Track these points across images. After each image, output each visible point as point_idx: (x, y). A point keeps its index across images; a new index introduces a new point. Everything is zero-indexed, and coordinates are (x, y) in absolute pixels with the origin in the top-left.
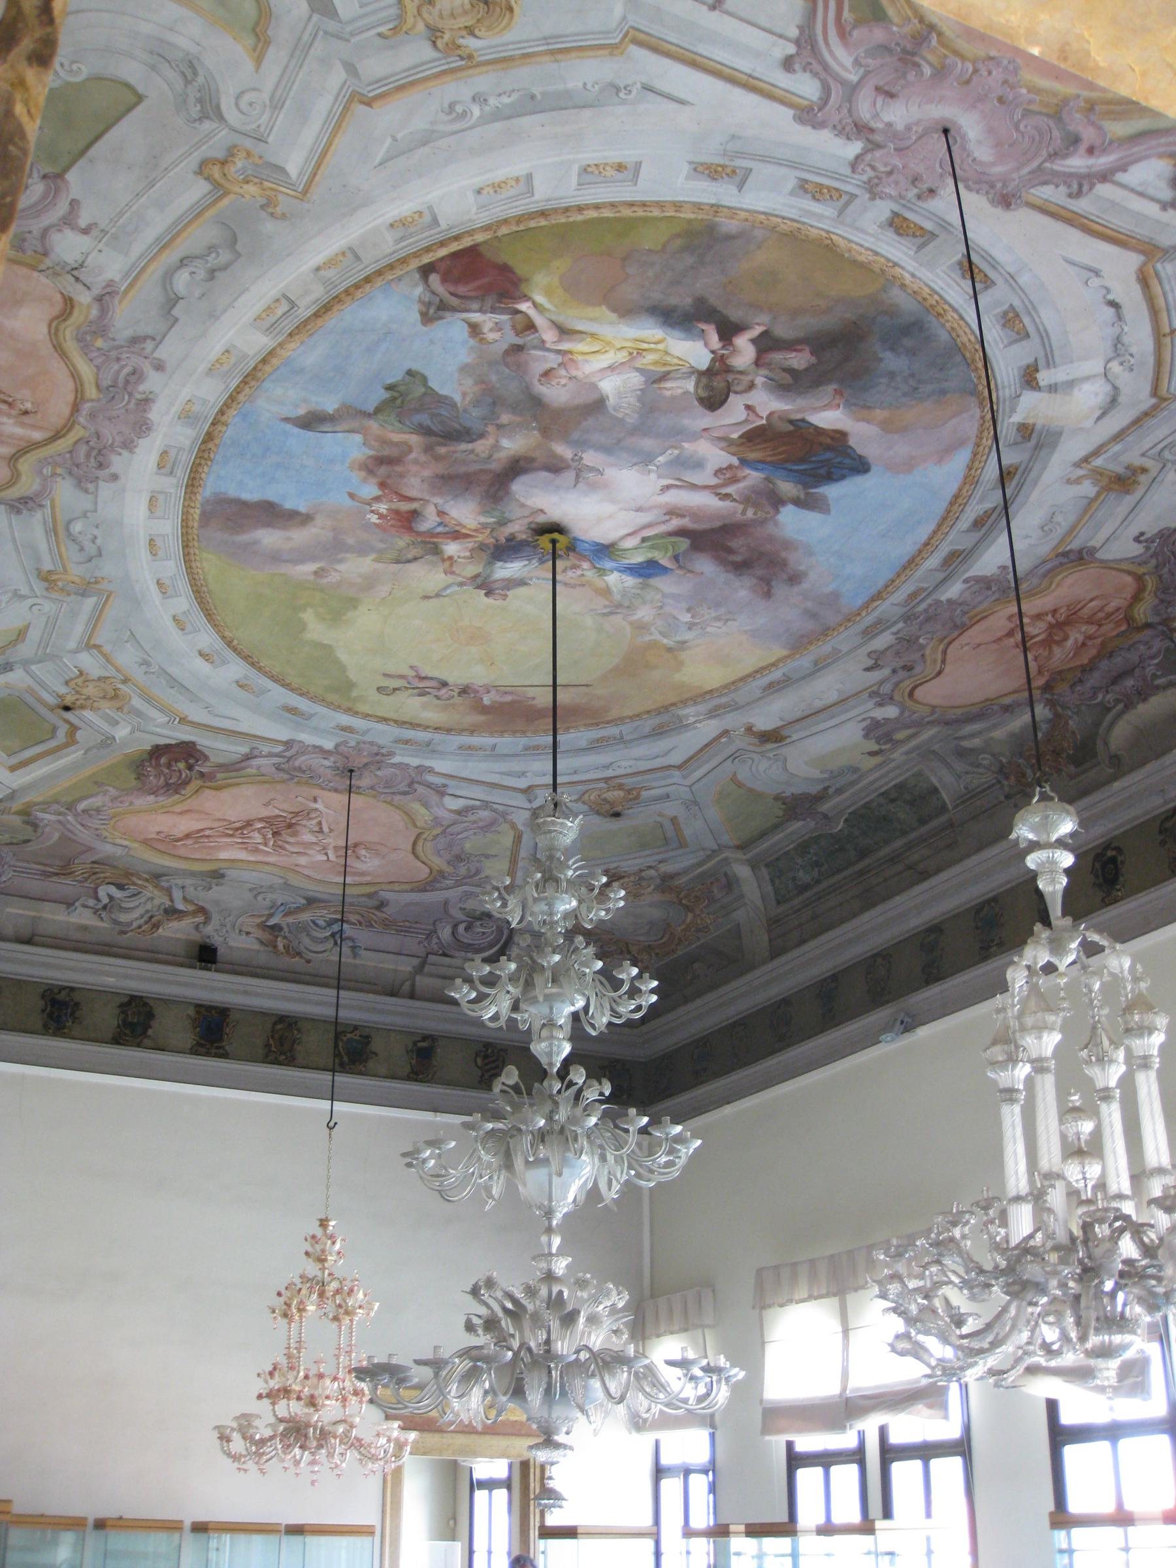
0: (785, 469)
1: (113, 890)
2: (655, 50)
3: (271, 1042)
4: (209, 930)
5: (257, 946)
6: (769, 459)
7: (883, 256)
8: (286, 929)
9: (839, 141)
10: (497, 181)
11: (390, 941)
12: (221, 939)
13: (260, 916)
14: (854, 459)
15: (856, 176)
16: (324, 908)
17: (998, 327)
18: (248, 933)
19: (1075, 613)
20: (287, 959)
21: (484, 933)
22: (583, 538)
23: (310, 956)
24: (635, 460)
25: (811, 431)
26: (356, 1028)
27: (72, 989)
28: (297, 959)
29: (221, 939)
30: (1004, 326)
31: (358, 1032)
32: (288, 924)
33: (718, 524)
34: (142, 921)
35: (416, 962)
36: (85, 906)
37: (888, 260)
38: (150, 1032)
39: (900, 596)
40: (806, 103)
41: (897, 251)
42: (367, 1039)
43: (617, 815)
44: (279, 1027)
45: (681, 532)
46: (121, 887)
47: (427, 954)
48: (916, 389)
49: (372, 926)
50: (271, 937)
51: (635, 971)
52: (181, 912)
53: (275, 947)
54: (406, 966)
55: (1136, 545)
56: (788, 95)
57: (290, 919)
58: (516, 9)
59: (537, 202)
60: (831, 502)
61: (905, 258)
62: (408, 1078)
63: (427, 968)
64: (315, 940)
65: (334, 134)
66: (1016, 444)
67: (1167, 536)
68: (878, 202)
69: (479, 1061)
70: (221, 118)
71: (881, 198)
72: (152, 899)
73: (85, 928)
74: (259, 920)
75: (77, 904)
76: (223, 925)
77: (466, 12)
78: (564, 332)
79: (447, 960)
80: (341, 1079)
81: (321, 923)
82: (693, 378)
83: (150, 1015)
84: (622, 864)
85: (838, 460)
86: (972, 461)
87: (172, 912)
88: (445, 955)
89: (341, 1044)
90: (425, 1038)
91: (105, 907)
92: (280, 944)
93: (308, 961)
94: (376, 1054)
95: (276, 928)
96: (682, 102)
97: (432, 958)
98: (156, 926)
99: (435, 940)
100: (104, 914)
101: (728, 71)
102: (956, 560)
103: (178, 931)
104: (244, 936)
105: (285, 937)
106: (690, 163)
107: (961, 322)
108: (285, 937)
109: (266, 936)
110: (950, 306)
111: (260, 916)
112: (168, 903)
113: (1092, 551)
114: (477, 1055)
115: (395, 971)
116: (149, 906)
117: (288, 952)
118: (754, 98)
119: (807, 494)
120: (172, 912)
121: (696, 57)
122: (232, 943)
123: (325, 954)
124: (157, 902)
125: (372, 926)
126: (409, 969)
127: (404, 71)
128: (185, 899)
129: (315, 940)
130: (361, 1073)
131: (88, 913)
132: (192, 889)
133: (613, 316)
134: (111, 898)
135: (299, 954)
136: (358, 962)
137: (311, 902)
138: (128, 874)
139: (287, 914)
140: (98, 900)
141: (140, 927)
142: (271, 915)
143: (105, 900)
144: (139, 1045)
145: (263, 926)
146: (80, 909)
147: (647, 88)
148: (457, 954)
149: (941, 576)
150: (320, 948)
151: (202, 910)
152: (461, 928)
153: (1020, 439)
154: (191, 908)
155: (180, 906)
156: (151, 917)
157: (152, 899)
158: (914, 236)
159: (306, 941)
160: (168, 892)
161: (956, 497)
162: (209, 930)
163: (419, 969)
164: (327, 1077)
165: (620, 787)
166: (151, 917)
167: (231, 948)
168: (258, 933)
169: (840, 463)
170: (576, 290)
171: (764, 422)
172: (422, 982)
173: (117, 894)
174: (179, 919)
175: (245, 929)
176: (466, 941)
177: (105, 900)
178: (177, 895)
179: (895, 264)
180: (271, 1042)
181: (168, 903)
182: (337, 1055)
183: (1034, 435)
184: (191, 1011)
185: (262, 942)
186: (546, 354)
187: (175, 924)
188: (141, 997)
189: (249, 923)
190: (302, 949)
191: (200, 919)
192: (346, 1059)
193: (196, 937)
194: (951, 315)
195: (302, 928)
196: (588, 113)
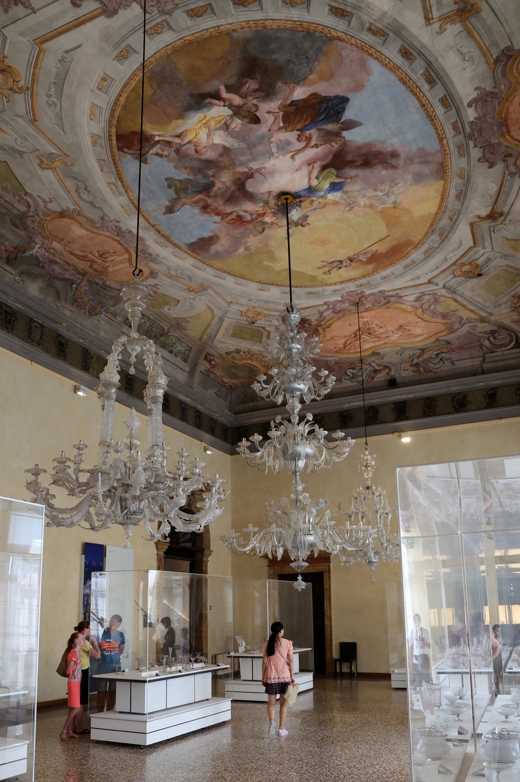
0: (318, 122)
1: (351, 371)
2: (48, 40)
3: (425, 409)
4: (392, 373)
5: (413, 374)
6: (307, 123)
7: (211, 28)
8: (421, 363)
9: (129, 10)
10: (89, 112)
11: (465, 354)
12: (398, 375)
13: (409, 362)
14: (336, 99)
16: (430, 351)
18: (407, 370)
20: (426, 374)
21: (504, 338)
22: (299, 190)
24: (267, 156)
25: (302, 102)
26: (460, 393)
27: (348, 410)
28: (430, 373)
29: (398, 375)
30: (293, 6)
31: (461, 395)
32: (421, 361)
34: (367, 378)
35: (480, 359)
36: (345, 379)
37: (214, 28)
38: (378, 418)
39: (449, 132)
41: (207, 23)
42: (465, 397)
43: (480, 275)
44: (427, 402)
45: (324, 168)
46: (353, 369)
47: (484, 354)
48: (308, 58)
49: (454, 351)
50: (417, 368)
52: (379, 370)
53: (420, 371)
54: (477, 362)
56: (93, 13)
57: (421, 359)
58: (11, 65)
59: (107, 108)
60: (356, 120)
61: (214, 22)
62: (486, 408)
63: (487, 360)
64: (435, 364)
65: (45, 135)
71: (173, 12)
72: (366, 369)
73: (347, 387)
74: (409, 364)
75: (342, 379)
76: (397, 370)
77: (6, 78)
78: (179, 136)
79: (494, 354)
83: (377, 412)
85: (330, 104)
88: (492, 352)
89: (454, 402)
90: (491, 389)
91: (352, 377)
92: (422, 369)
93: (435, 373)
94: (470, 402)
95: (417, 364)
96: (79, 46)
97: (487, 355)
98: (373, 378)
99: (484, 348)
100: (353, 380)
103: (381, 377)
104: (406, 371)
105: (422, 367)
107: (276, 21)
108: (422, 367)
109: (414, 368)
110: (262, 20)
111: (409, 362)
112: (373, 369)
115: (473, 365)
116: (367, 372)
117: (426, 372)
118: (89, 25)
119: (342, 123)
120: (376, 371)
121: (59, 30)
122: (403, 376)
123: (441, 368)
124: (369, 369)
125: (454, 351)
126: (479, 363)
127: (26, 105)
128: (377, 365)
129: (435, 364)
130: (465, 411)
132: (377, 361)
134: (353, 373)
135: (430, 371)
136: (456, 367)
137: (423, 350)
139: (418, 358)
140: (349, 376)
141: (367, 380)
142: (413, 360)
143: (351, 375)
144: (375, 424)
145: (412, 365)
146: (344, 381)
148: (497, 350)
149: (453, 112)
150: (438, 366)
151: (386, 367)
154: (382, 368)
155: (378, 368)
156: (370, 376)
157: (366, 369)
158: (205, 11)
159: (431, 365)
160: (370, 364)
162: (392, 373)
163: (483, 361)
166: (370, 376)
167: (403, 377)
168: (411, 369)
169: (332, 104)
170: (166, 119)
171: (282, 113)
173: (354, 371)
174: (380, 373)
175: (406, 368)
176: (498, 343)
177: (351, 375)
178: (374, 365)
179: (218, 27)
180: (425, 409)
181: (373, 369)
182: (454, 407)
183: (386, 31)
184: (392, 406)
185: (413, 371)
186: (186, 146)
188: (373, 406)
189: (406, 366)
190: (431, 369)
191: (387, 370)
192: (457, 407)
193: (389, 377)
194: (267, 23)
195: (428, 360)
196: (70, 73)
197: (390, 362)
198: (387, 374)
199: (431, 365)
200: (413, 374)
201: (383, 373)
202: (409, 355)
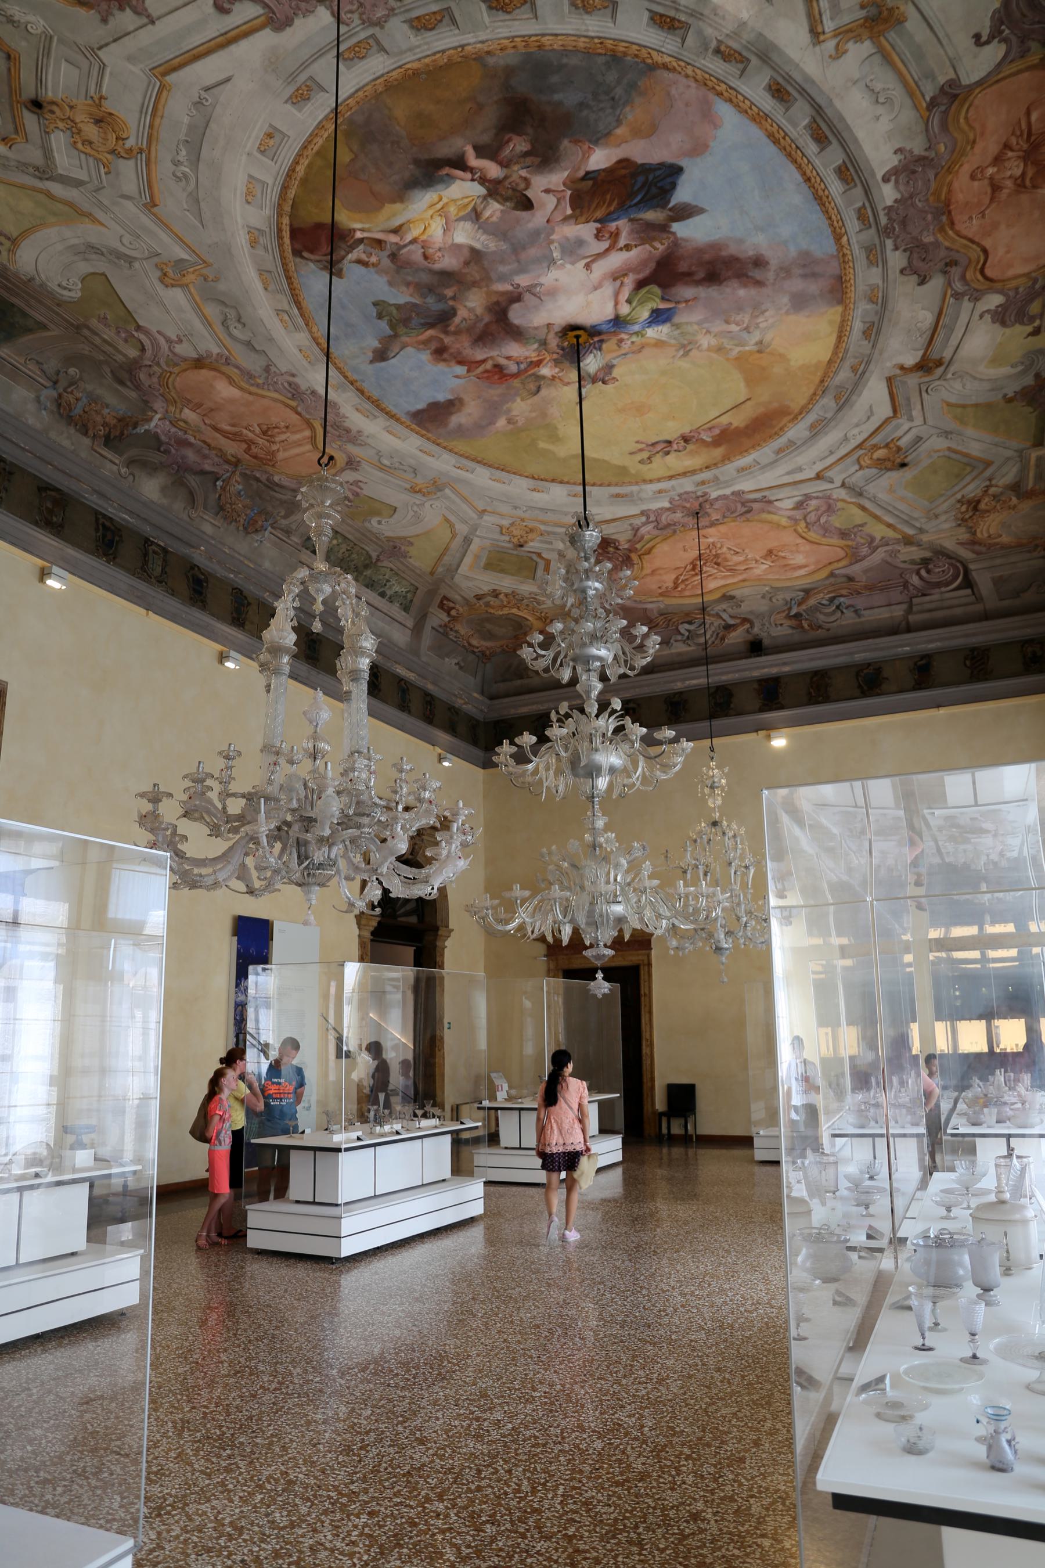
1: (687, 626)
4: (756, 630)
5: (790, 631)
11: (879, 598)
15: (353, 25)
17: (586, 17)
19: (1030, 134)
23: (828, 626)
26: (869, 665)
30: (587, 13)
33: (652, 265)
35: (904, 606)
37: (455, 48)
40: (263, 18)
41: (444, 41)
42: (879, 670)
43: (903, 465)
45: (640, 285)
46: (690, 623)
48: (613, 99)
51: (645, 629)
54: (898, 611)
55: (988, 49)
57: (804, 607)
62: (914, 689)
63: (915, 609)
66: (743, 72)
67: (1003, 21)
68: (387, 26)
69: (968, 663)
70: (136, 259)
73: (680, 654)
79: (927, 598)
80: (716, 723)
81: (824, 602)
82: (491, 201)
83: (731, 695)
84: (965, 492)
86: (737, 106)
87: (728, 627)
88: (924, 595)
90: (922, 657)
92: (805, 625)
95: (798, 616)
96: (228, 80)
97: (915, 601)
98: (723, 639)
101: (212, 43)
102: (851, 171)
103: (737, 637)
106: (286, 102)
109: (793, 623)
113: (953, 83)
114: (966, 658)
118: (244, 45)
120: (728, 627)
129: (825, 614)
131: (680, 644)
133: (398, 206)
135: (820, 627)
138: (687, 615)
139: (799, 604)
142: (790, 609)
145: (789, 617)
147: (207, 89)
149: (858, 191)
150: (832, 619)
151: (745, 620)
152: (923, 572)
153: (741, 66)
155: (731, 622)
158: (441, 21)
159: (821, 617)
161: (770, 135)
162: (756, 630)
163: (910, 610)
164: (706, 724)
165: (875, 447)
168: (788, 623)
171: (569, 192)
172: (912, 618)
173: (691, 627)
178: (725, 616)
179: (463, 46)
184: (756, 686)
187: (733, 634)
189: (780, 618)
191: (747, 626)
193: (750, 638)
195: (815, 609)
196: (212, 125)
197: (751, 612)
198: (748, 631)
199: (821, 617)
200: (790, 631)
201: (740, 630)
202: (784, 599)
